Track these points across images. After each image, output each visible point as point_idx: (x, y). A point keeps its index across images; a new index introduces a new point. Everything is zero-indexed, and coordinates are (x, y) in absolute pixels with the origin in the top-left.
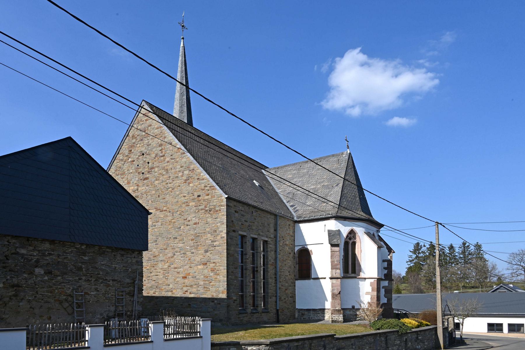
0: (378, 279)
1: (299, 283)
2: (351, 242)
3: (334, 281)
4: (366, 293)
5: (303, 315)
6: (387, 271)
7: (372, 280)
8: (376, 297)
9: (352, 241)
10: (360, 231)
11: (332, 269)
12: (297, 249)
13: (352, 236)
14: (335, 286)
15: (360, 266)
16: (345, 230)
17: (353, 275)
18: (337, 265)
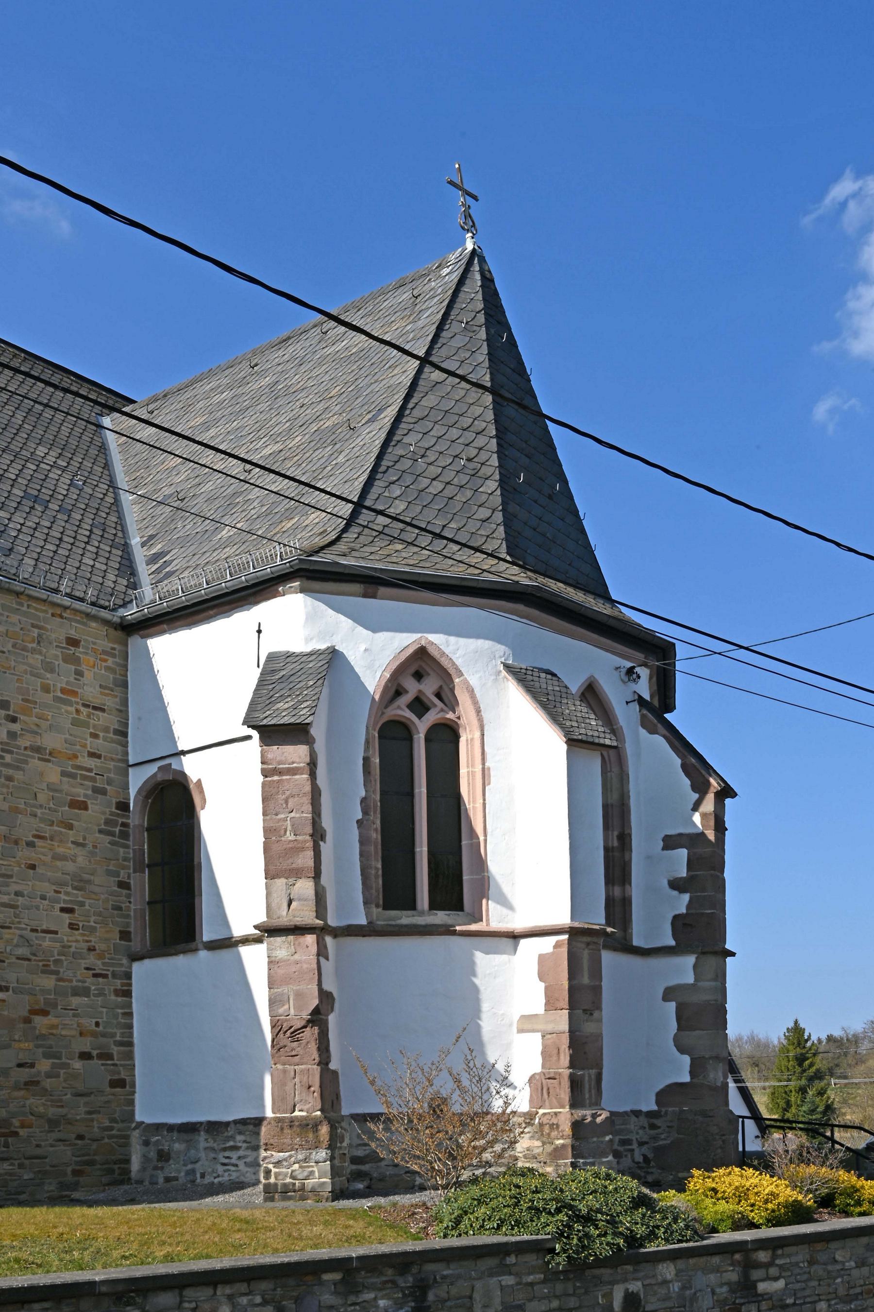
0: (574, 933)
1: (155, 979)
2: (422, 726)
3: (282, 946)
4: (513, 1011)
5: (164, 1156)
6: (686, 897)
7: (547, 944)
8: (565, 1040)
9: (431, 717)
10: (477, 657)
11: (270, 875)
12: (137, 780)
13: (428, 688)
14: (287, 980)
15: (481, 864)
16: (373, 652)
17: (441, 917)
18: (296, 849)
